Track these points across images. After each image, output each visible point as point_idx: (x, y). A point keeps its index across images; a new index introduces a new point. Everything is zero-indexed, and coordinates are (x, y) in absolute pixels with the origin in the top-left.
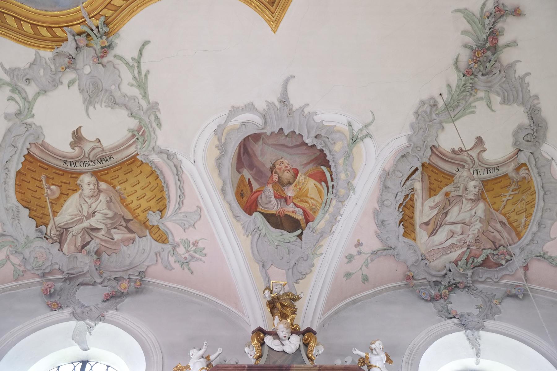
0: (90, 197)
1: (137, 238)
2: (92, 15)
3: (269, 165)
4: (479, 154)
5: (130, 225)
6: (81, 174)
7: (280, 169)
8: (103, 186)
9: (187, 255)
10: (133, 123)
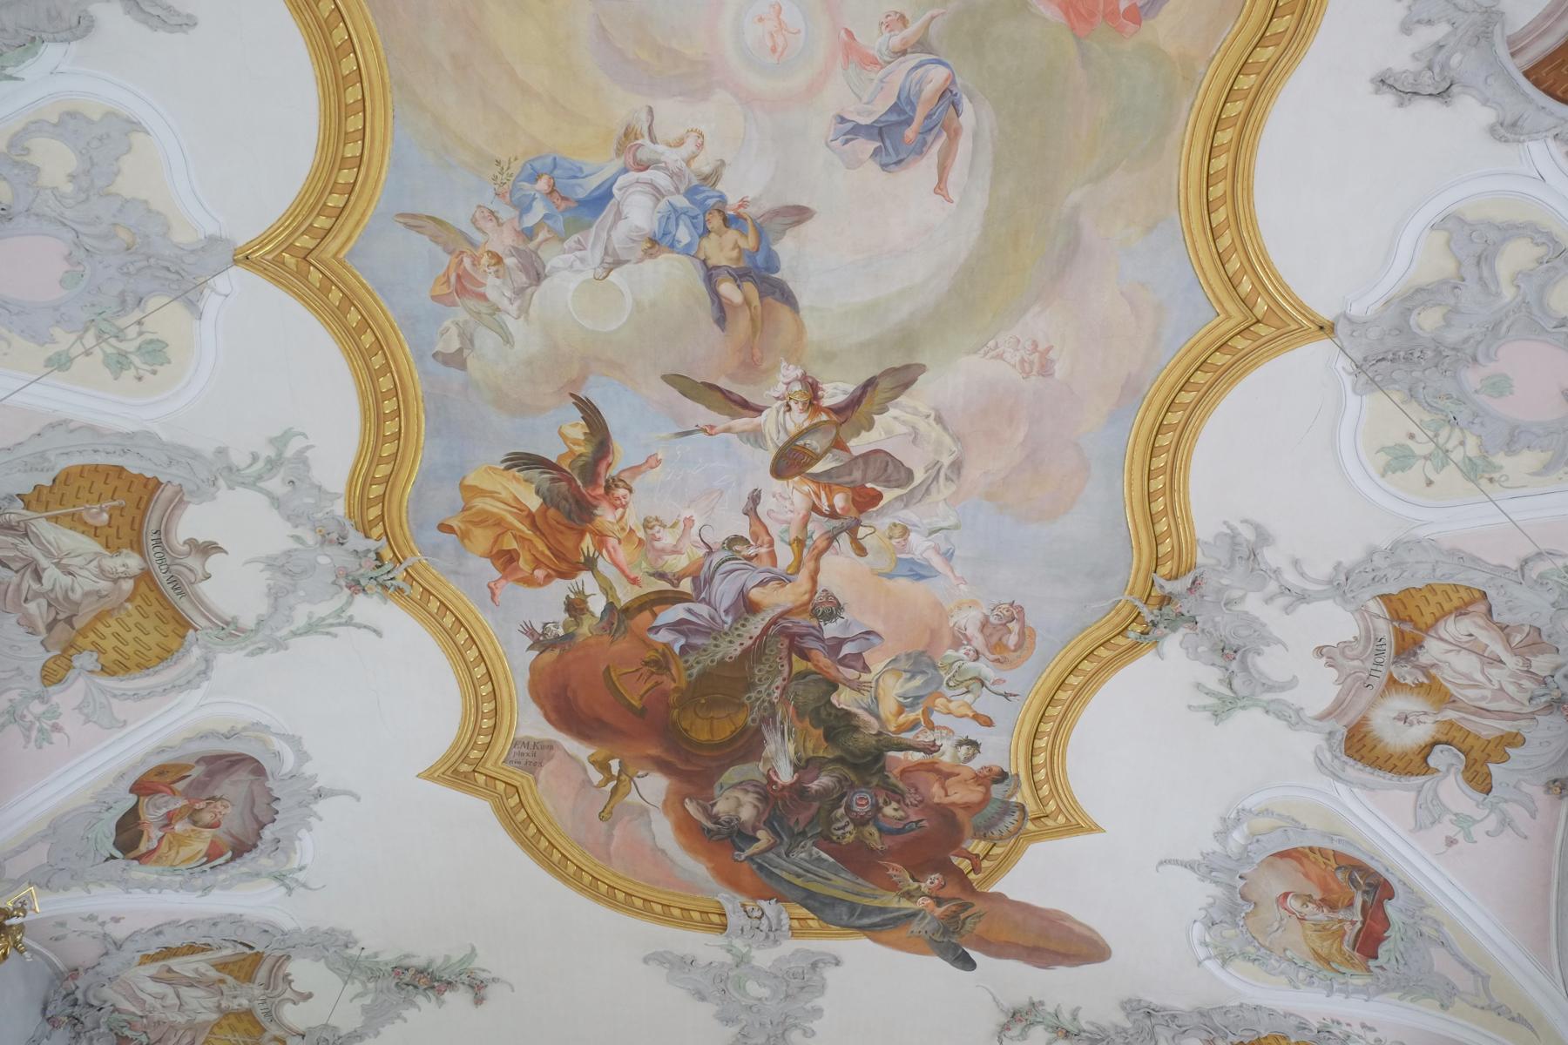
0: (100, 567)
1: (41, 638)
2: (409, 570)
3: (218, 794)
4: (288, 999)
5: (60, 627)
6: (141, 554)
7: (215, 807)
8: (128, 585)
9: (30, 718)
10: (248, 621)
